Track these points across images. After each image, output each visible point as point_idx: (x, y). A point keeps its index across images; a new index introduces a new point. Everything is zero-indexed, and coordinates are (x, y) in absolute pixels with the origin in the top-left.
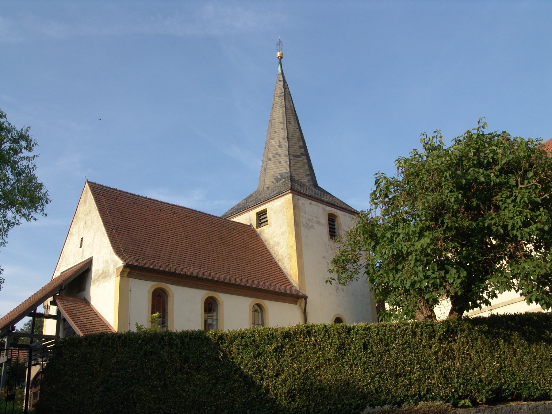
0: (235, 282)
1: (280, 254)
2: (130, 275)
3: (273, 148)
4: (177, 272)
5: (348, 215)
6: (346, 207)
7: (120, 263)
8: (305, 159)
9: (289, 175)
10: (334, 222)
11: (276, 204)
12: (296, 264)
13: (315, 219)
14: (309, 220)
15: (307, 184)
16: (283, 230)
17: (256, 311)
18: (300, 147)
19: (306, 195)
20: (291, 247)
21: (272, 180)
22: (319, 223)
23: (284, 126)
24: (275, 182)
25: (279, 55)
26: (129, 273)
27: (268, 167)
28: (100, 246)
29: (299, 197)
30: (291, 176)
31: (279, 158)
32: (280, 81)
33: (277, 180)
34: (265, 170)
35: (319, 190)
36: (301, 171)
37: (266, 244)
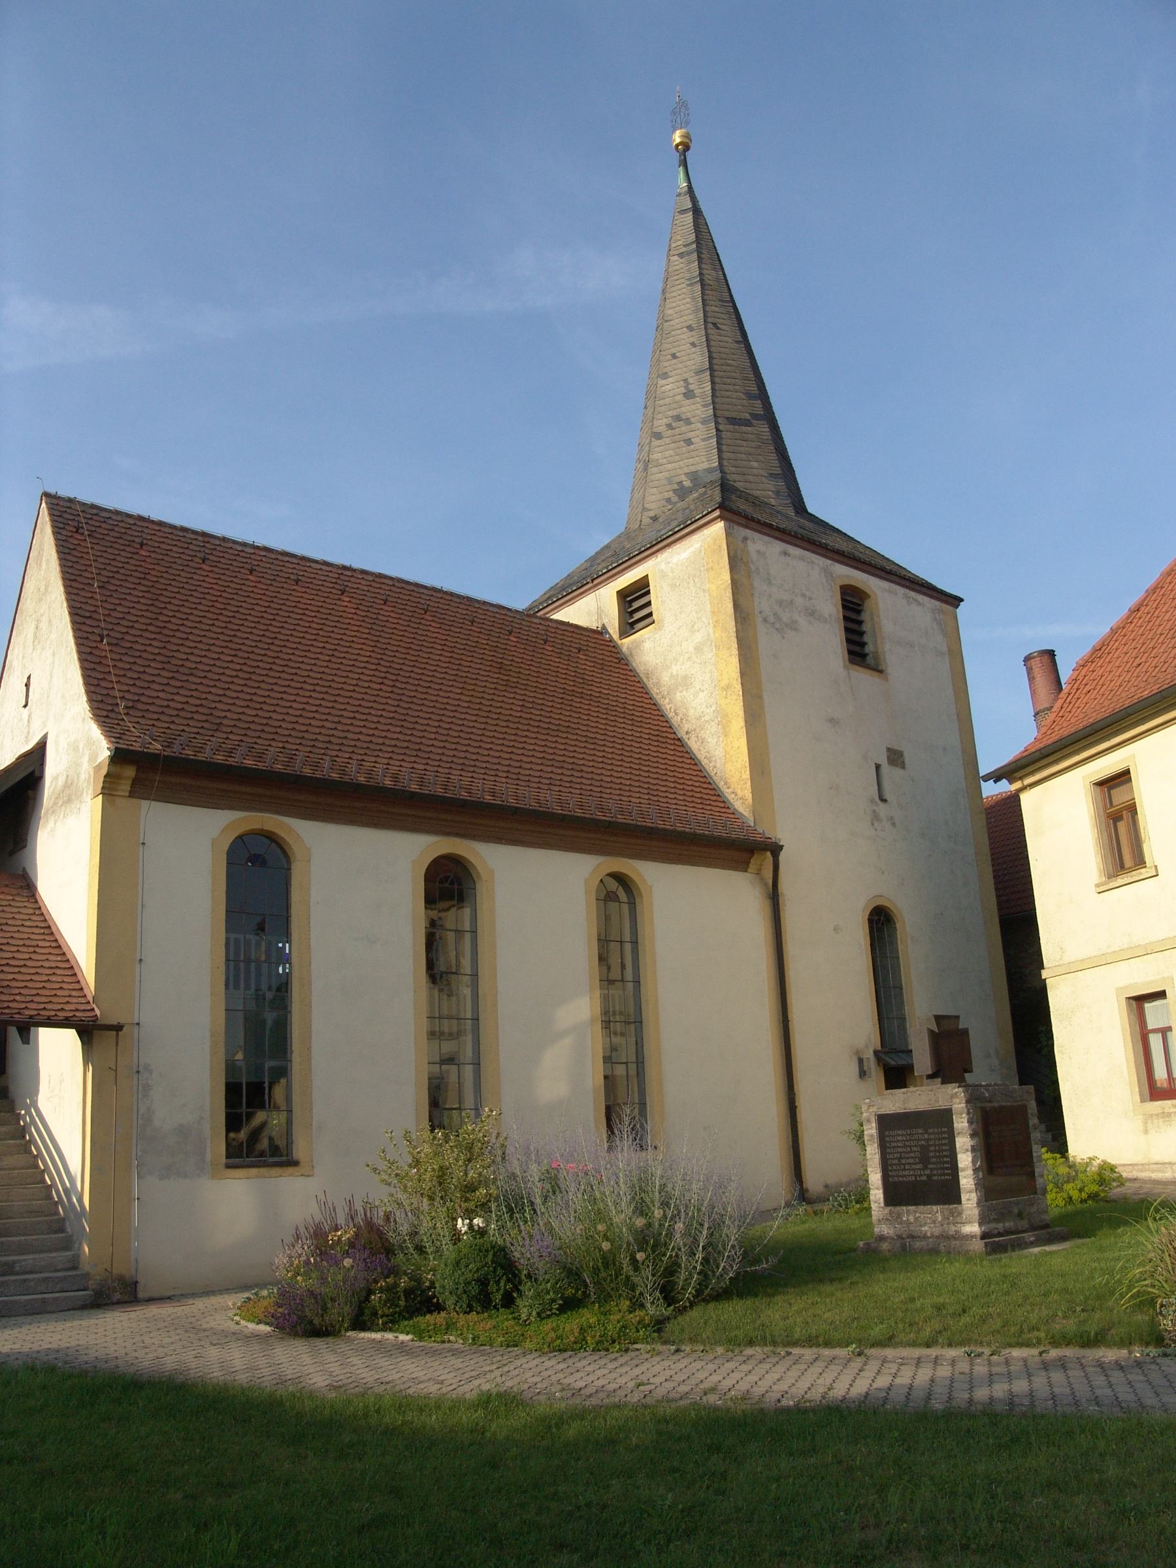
0: (534, 805)
1: (691, 712)
2: (140, 790)
3: (667, 401)
4: (346, 779)
5: (901, 591)
6: (895, 569)
7: (103, 749)
8: (765, 429)
9: (945, 1398)
10: (859, 612)
11: (675, 559)
12: (742, 743)
13: (799, 601)
14: (780, 603)
15: (773, 502)
16: (698, 638)
17: (608, 897)
18: (750, 396)
19: (770, 526)
20: (727, 688)
21: (667, 495)
22: (811, 613)
23: (699, 336)
24: (675, 499)
25: (678, 140)
26: (135, 782)
27: (655, 456)
28: (63, 697)
29: (748, 533)
30: (722, 478)
31: (684, 429)
32: (683, 212)
33: (682, 492)
34: (645, 469)
35: (812, 521)
36: (755, 464)
37: (650, 684)
